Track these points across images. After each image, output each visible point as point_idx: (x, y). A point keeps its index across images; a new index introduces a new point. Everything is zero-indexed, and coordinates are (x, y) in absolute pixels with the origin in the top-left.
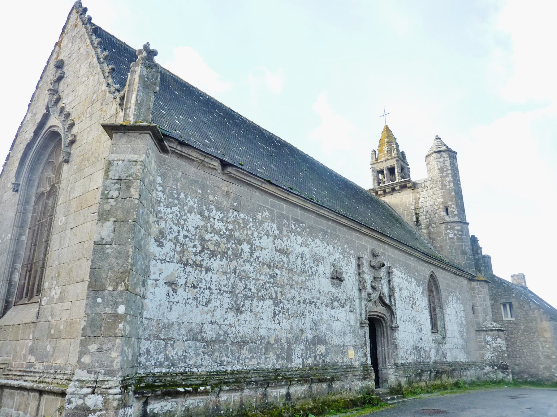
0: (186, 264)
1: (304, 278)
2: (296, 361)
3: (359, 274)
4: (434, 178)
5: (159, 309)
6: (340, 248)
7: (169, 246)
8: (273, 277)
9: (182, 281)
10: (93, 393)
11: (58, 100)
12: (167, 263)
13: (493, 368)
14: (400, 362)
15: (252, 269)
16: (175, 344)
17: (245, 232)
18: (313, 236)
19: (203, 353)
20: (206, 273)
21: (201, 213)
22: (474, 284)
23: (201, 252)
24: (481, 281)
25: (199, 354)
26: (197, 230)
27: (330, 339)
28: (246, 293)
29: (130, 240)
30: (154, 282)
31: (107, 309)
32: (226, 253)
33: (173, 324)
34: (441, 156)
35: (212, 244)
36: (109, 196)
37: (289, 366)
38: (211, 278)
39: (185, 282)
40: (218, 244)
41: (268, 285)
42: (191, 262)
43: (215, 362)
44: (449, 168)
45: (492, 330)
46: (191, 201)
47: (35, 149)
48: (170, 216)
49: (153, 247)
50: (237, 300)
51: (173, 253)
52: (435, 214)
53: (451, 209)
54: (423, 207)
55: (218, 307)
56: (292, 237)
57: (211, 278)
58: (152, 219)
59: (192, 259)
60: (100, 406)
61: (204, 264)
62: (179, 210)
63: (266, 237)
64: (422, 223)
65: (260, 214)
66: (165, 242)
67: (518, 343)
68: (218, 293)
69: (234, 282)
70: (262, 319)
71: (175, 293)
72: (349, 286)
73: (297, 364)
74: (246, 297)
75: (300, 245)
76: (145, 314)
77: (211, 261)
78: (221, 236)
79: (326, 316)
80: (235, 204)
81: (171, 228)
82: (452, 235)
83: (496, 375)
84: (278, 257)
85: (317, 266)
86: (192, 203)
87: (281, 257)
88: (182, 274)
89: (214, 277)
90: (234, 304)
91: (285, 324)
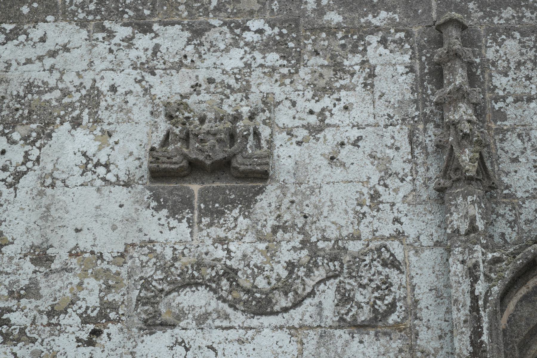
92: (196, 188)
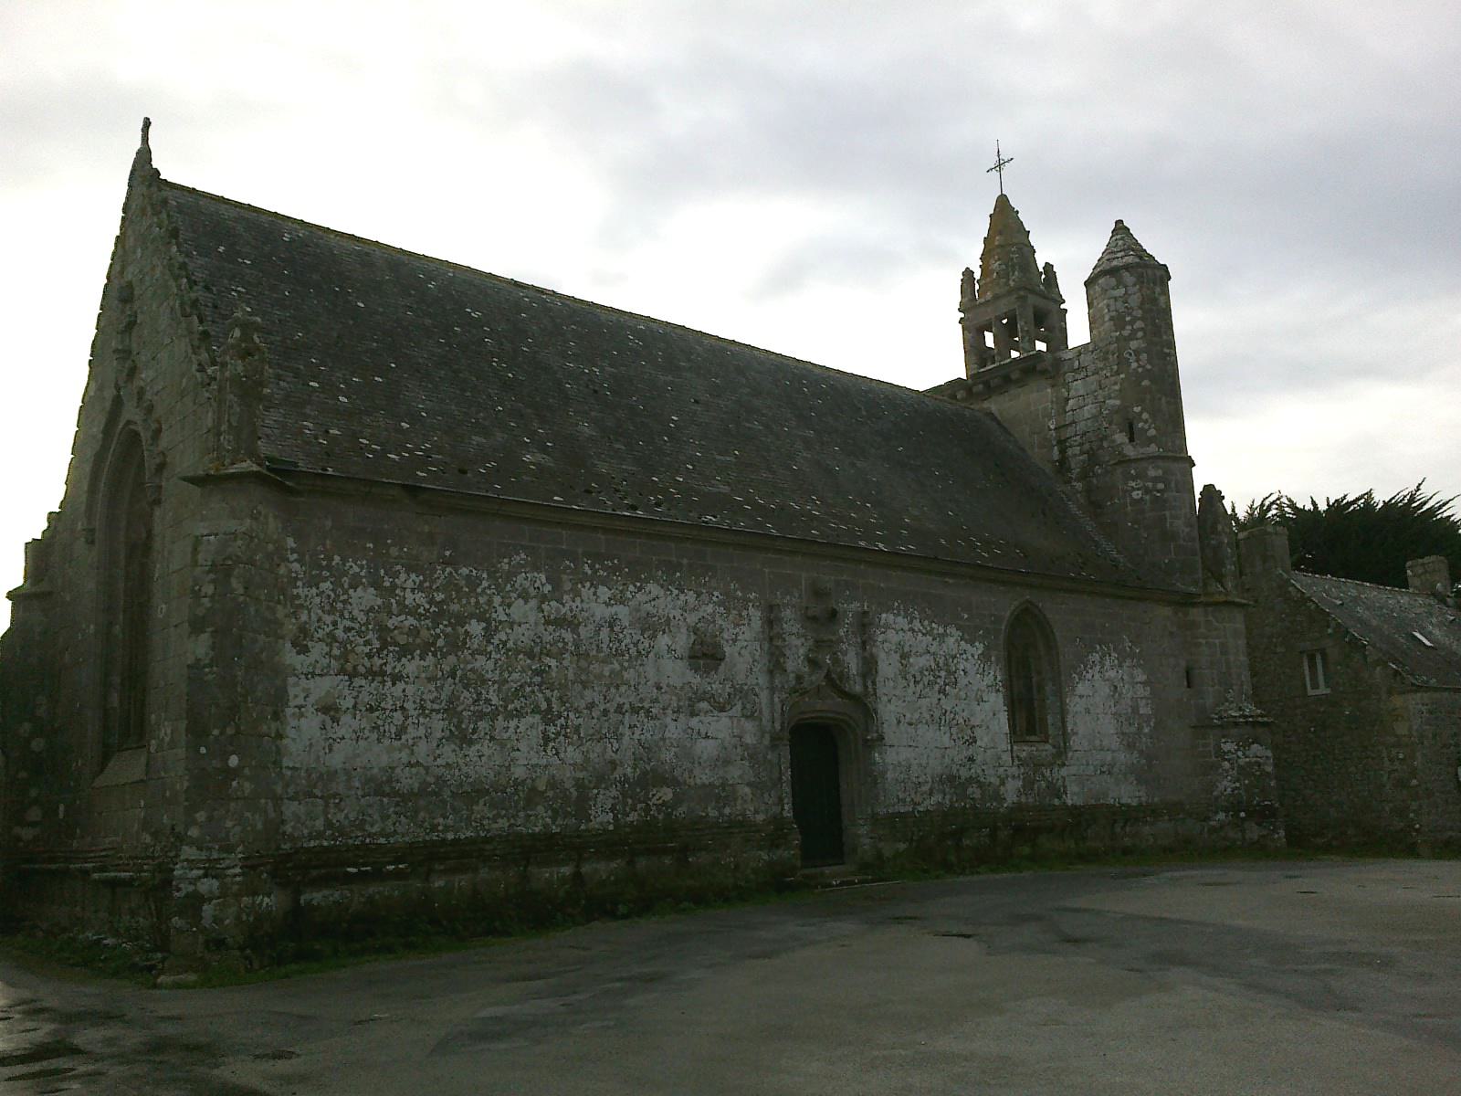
0: (353, 675)
1: (616, 666)
2: (598, 820)
3: (771, 639)
4: (1100, 345)
5: (309, 751)
6: (716, 593)
7: (317, 650)
8: (538, 673)
9: (349, 703)
10: (206, 876)
11: (133, 372)
12: (317, 678)
13: (1236, 815)
14: (881, 811)
15: (490, 664)
16: (343, 803)
17: (473, 601)
18: (640, 580)
19: (396, 813)
20: (394, 684)
21: (376, 584)
22: (1196, 614)
23: (379, 651)
24: (1217, 604)
25: (389, 817)
26: (370, 614)
27: (686, 775)
28: (480, 708)
29: (236, 659)
30: (297, 710)
31: (214, 762)
32: (434, 644)
33: (336, 771)
34: (1120, 283)
35: (401, 633)
36: (203, 594)
37: (583, 827)
38: (404, 691)
39: (352, 704)
40: (414, 632)
41: (528, 689)
42: (361, 669)
43: (421, 826)
44: (1139, 313)
45: (1236, 724)
46: (354, 566)
47: (114, 450)
48: (318, 600)
49: (290, 657)
50: (461, 722)
51: (328, 661)
52: (1102, 440)
53: (1140, 425)
54: (1075, 422)
55: (420, 738)
56: (586, 591)
57: (404, 691)
58: (281, 612)
59: (363, 665)
60: (217, 893)
61: (389, 669)
62: (331, 587)
63: (521, 601)
64: (1073, 466)
65: (506, 560)
66: (310, 644)
67: (1337, 752)
68: (419, 715)
69: (453, 693)
70: (518, 750)
71: (335, 724)
72: (741, 665)
73: (601, 823)
74: (481, 716)
75: (605, 603)
76: (286, 762)
77: (402, 663)
78: (419, 617)
79: (674, 731)
80: (448, 553)
81: (319, 620)
82: (1140, 492)
83: (1243, 831)
84: (549, 635)
85: (653, 637)
86: (356, 569)
87: (558, 634)
88: (346, 692)
89: (410, 689)
90: (453, 729)
91: (572, 754)
92: (702, 662)
